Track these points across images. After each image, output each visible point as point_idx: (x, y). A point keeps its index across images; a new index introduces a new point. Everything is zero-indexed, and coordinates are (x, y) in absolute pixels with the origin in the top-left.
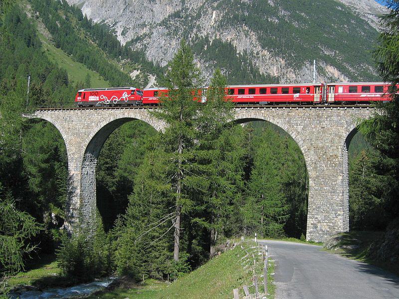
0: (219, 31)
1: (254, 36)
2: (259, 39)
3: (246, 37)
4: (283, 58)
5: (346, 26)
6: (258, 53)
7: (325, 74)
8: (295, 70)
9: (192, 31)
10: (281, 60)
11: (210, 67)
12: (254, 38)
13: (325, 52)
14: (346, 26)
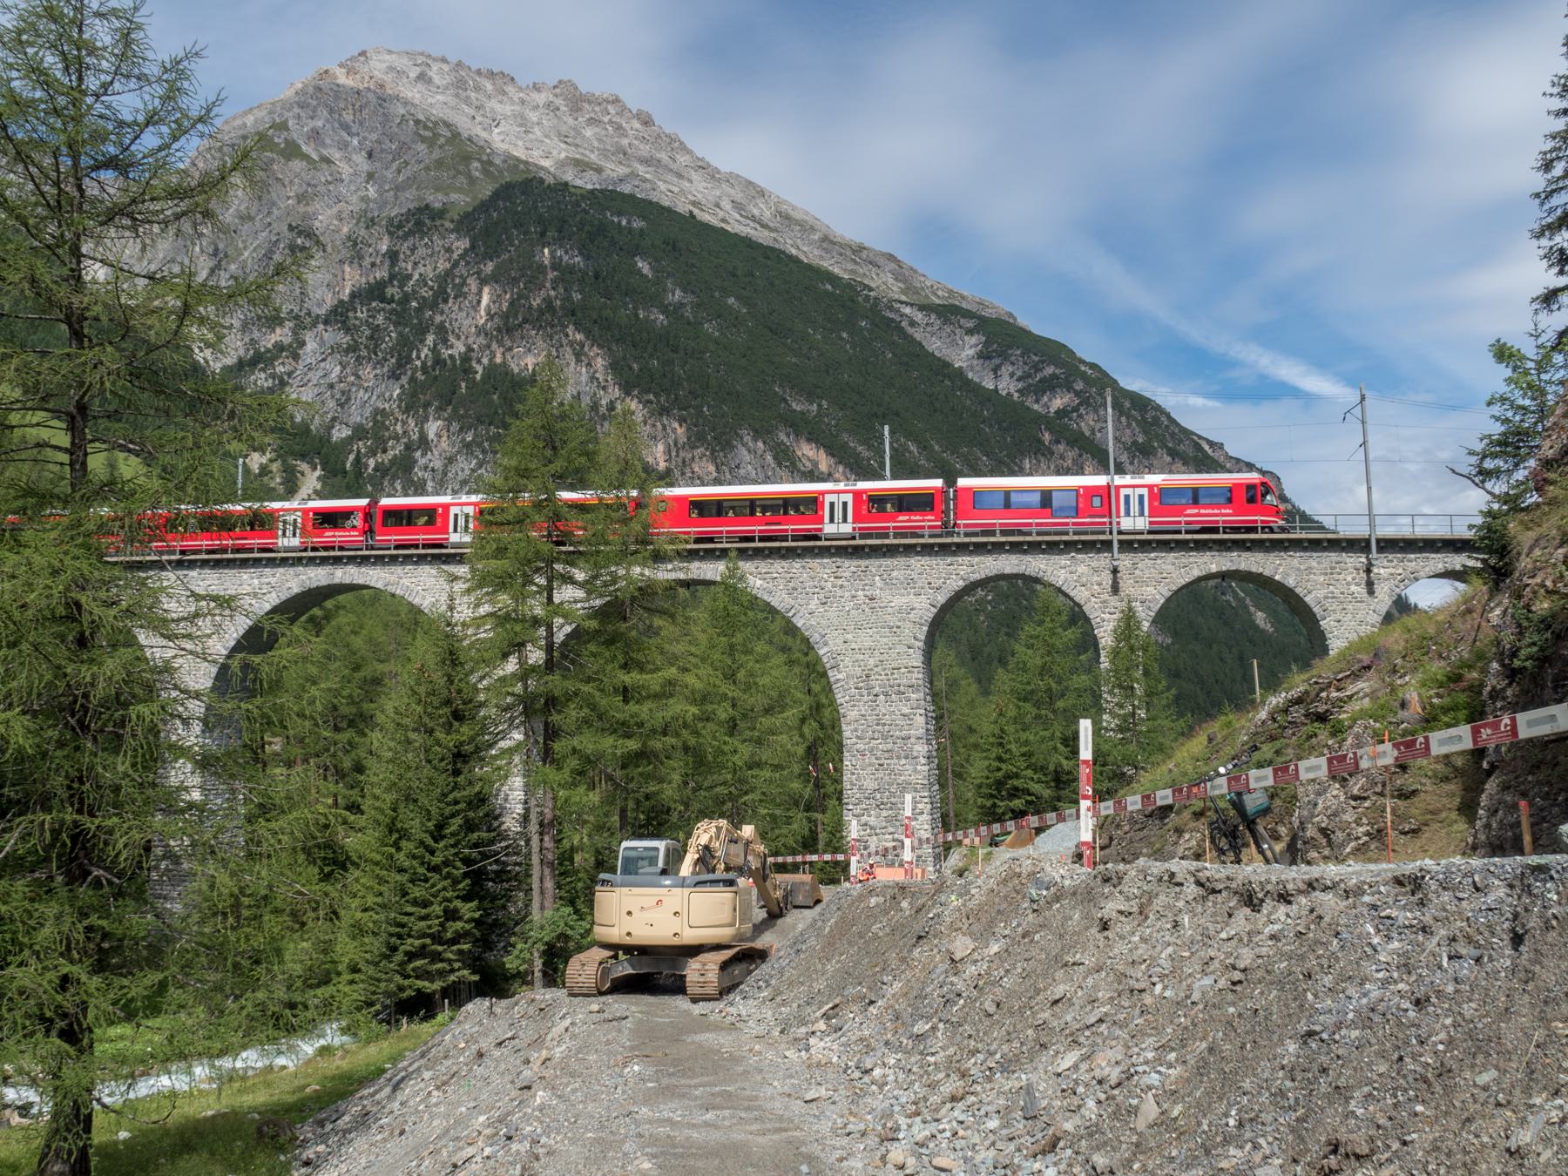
0: (500, 343)
1: (599, 360)
2: (615, 367)
3: (578, 361)
4: (682, 421)
5: (845, 335)
6: (611, 407)
7: (793, 464)
8: (713, 451)
9: (422, 341)
10: (676, 425)
11: (477, 443)
12: (600, 363)
13: (794, 405)
14: (845, 335)
